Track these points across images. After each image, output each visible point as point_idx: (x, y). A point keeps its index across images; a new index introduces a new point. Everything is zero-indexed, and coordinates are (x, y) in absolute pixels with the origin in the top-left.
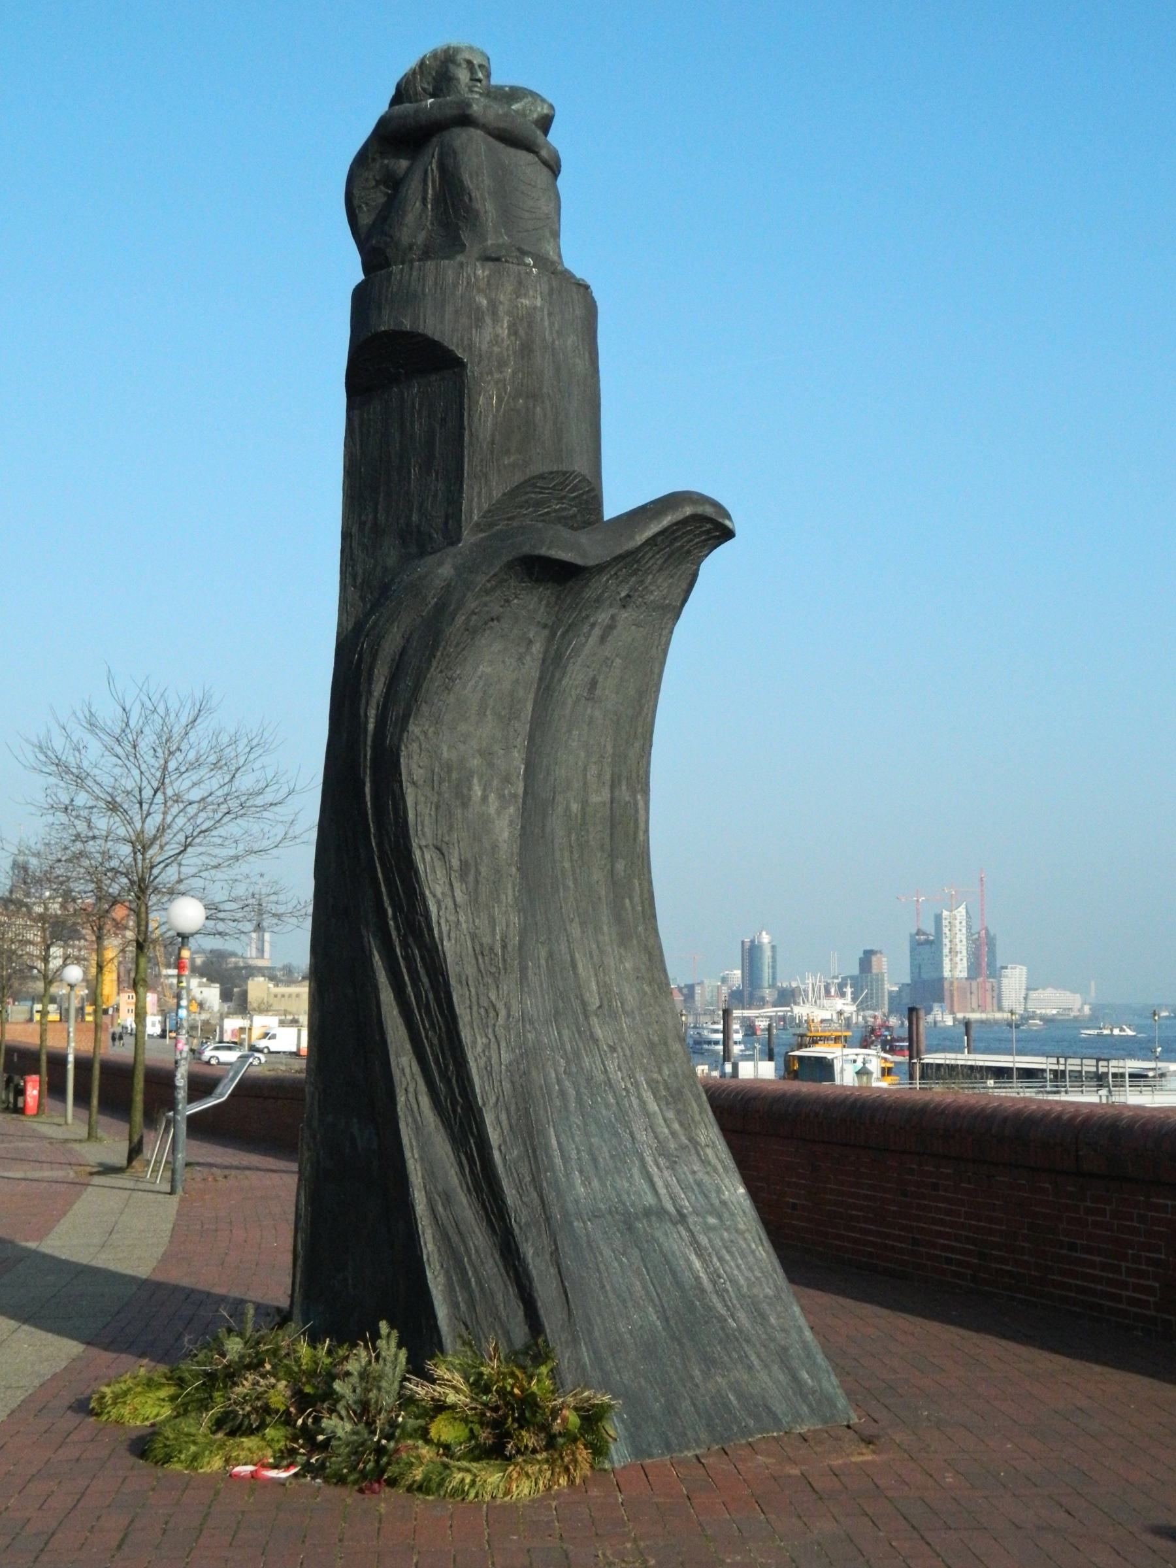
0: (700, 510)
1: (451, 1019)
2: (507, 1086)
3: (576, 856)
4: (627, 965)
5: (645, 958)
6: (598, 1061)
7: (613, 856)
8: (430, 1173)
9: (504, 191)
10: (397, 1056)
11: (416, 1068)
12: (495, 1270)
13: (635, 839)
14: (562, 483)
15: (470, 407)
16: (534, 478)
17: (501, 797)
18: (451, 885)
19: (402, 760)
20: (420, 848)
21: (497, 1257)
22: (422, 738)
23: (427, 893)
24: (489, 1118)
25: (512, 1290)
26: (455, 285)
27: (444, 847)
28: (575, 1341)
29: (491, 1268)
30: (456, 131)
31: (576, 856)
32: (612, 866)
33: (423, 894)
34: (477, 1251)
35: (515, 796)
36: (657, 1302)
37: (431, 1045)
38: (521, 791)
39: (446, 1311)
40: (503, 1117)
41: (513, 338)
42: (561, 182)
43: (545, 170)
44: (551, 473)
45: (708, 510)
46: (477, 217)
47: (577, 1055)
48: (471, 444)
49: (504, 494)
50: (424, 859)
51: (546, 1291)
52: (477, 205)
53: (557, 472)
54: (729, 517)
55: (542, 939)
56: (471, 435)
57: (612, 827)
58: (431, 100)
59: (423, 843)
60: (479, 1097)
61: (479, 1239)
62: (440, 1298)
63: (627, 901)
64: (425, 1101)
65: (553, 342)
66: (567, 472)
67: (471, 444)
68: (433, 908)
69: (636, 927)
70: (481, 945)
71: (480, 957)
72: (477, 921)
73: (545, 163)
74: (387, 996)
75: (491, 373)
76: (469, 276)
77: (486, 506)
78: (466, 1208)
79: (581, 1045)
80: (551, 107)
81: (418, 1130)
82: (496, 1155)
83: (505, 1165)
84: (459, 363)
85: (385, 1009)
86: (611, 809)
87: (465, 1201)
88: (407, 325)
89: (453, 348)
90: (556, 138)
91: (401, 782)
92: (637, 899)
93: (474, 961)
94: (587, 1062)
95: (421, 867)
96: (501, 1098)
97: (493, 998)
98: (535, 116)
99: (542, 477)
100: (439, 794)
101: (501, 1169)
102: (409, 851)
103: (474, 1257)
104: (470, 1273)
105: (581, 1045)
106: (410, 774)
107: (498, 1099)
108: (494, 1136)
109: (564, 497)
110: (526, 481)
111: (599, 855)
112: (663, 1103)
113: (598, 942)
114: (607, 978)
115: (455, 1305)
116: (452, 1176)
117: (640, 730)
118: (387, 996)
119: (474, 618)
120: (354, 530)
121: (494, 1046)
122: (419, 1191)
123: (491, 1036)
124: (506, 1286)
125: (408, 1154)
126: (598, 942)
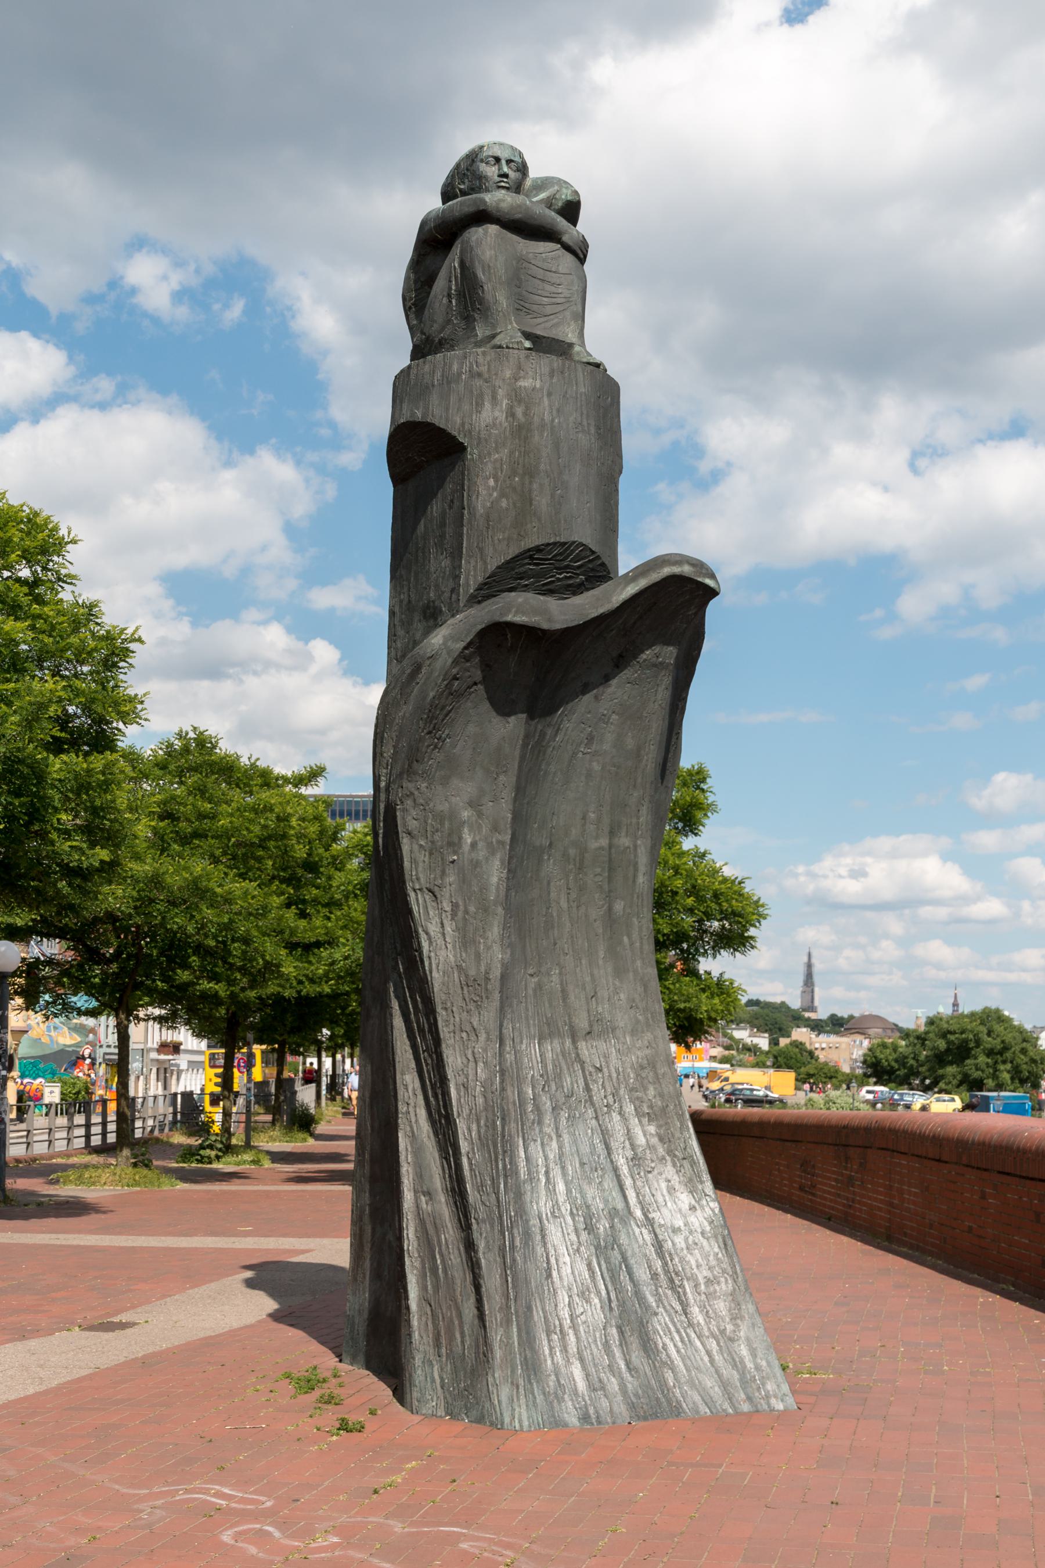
0: (676, 570)
1: (437, 1041)
2: (480, 1100)
3: (574, 895)
4: (622, 996)
5: (640, 989)
6: (581, 1082)
7: (610, 897)
8: (420, 1175)
9: (519, 277)
10: (403, 1074)
11: (417, 1084)
12: (459, 1260)
13: (634, 881)
14: (561, 554)
15: (469, 487)
16: (529, 550)
17: (490, 845)
18: (442, 924)
19: (398, 814)
20: (415, 890)
21: (462, 1249)
22: (416, 793)
23: (420, 930)
24: (461, 1125)
25: (469, 1277)
26: (460, 374)
27: (436, 889)
28: (508, 1322)
29: (456, 1258)
30: (473, 230)
31: (574, 895)
32: (610, 909)
33: (417, 932)
34: (446, 1243)
35: (501, 843)
36: (604, 1293)
37: (427, 1065)
38: (507, 838)
39: (417, 1293)
40: (474, 1127)
41: (510, 419)
42: (587, 266)
43: (569, 258)
44: (548, 544)
45: (686, 570)
46: (488, 309)
47: (559, 1076)
48: (470, 522)
49: (498, 567)
50: (417, 900)
51: (492, 1280)
52: (488, 296)
53: (555, 544)
54: (713, 576)
55: (531, 971)
56: (469, 513)
57: (611, 869)
58: (469, 841)
59: (417, 887)
60: (455, 1109)
61: (450, 1234)
62: (414, 1280)
63: (625, 939)
64: (422, 1113)
65: (553, 421)
66: (565, 543)
67: (470, 522)
68: (425, 945)
69: (634, 962)
70: (467, 976)
71: (465, 988)
72: (464, 955)
73: (567, 248)
74: (398, 1022)
75: (489, 454)
76: (471, 364)
77: (480, 579)
78: (443, 1207)
79: (565, 1067)
80: (576, 193)
81: (413, 1137)
82: (465, 1161)
83: (471, 1170)
84: (461, 448)
85: (396, 1033)
86: (610, 854)
87: (443, 1200)
88: (419, 415)
89: (455, 433)
90: (585, 226)
91: (397, 832)
92: (635, 935)
93: (460, 991)
94: (567, 1081)
95: (415, 908)
96: (473, 1111)
97: (475, 1024)
98: (560, 204)
99: (538, 549)
100: (433, 842)
101: (467, 1172)
102: (406, 895)
103: (443, 1247)
104: (439, 1262)
105: (565, 1067)
106: (404, 825)
107: (471, 1110)
108: (464, 1146)
109: (567, 567)
110: (521, 554)
111: (597, 896)
112: (645, 1120)
113: (592, 975)
114: (600, 1009)
115: (424, 1288)
116: (437, 1181)
117: (639, 780)
118: (398, 1022)
119: (456, 683)
120: (397, 609)
121: (472, 1064)
122: (409, 1190)
123: (470, 1057)
124: (465, 1274)
125: (402, 1158)
126: (592, 975)
